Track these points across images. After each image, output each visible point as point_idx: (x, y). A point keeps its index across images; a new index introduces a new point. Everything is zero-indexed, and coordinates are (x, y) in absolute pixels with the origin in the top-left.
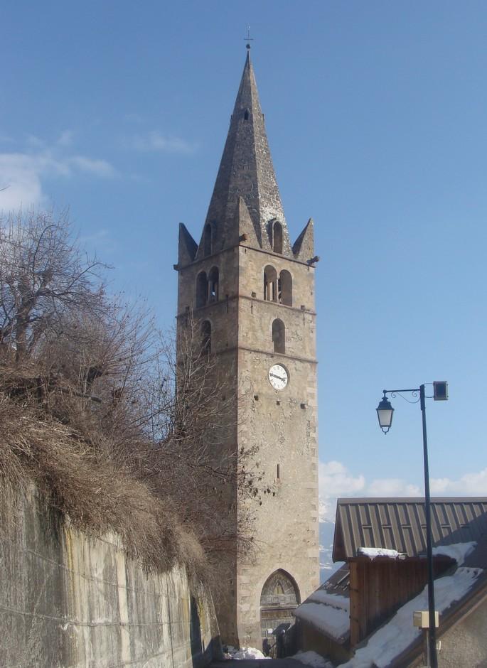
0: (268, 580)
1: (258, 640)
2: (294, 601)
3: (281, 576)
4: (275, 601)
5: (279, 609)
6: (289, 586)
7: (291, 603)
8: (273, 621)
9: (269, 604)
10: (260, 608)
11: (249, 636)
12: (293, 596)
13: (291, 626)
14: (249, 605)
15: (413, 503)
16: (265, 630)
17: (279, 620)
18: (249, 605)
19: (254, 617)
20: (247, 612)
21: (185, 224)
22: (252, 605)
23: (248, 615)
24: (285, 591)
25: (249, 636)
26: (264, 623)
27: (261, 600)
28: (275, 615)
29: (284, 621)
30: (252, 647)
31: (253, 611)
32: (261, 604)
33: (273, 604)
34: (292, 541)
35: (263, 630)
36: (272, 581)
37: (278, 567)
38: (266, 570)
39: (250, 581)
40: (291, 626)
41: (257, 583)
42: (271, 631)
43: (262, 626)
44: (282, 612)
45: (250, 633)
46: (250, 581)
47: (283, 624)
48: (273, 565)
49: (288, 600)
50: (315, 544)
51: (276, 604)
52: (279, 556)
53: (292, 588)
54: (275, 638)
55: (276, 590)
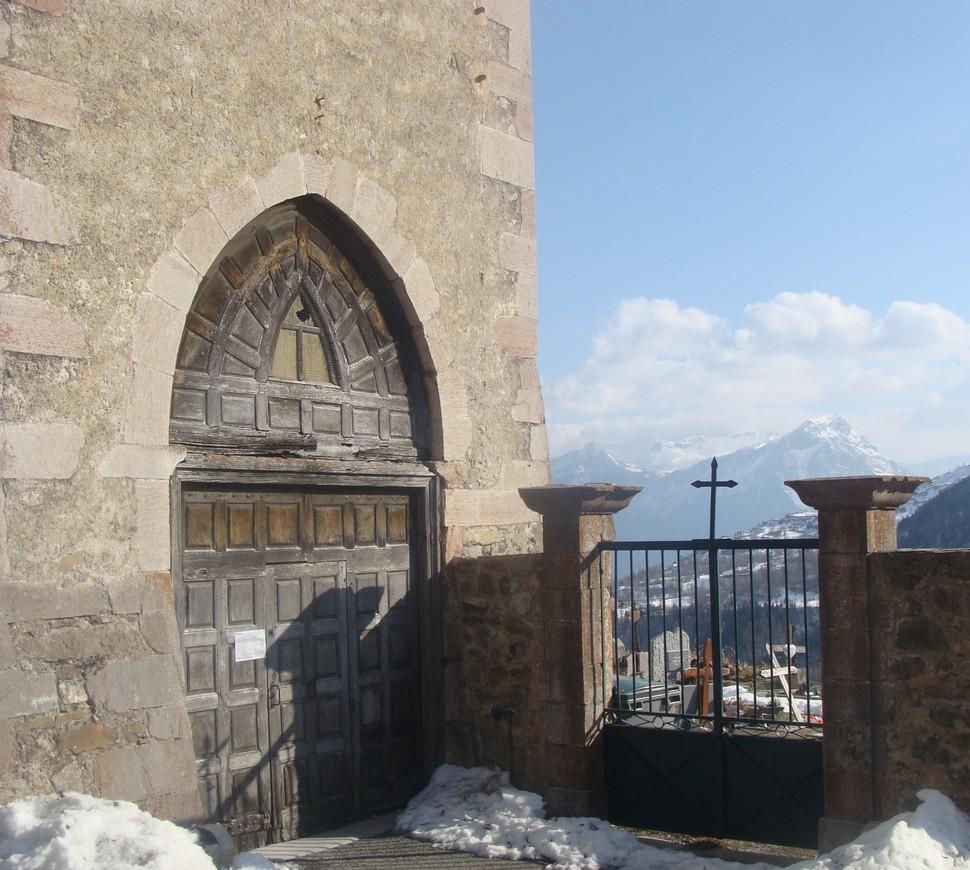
0: (232, 264)
1: (159, 726)
2: (398, 439)
3: (324, 259)
4: (282, 426)
5: (313, 487)
6: (372, 339)
7: (384, 455)
8: (267, 572)
9: (239, 446)
10: (170, 461)
11: (76, 696)
12: (394, 404)
13: (384, 609)
14: (71, 432)
15: (373, 588)
16: (211, 636)
17: (307, 569)
18: (71, 432)
19: (124, 530)
20: (58, 492)
21: (339, 201)
22: (100, 433)
23: (64, 517)
24: (348, 369)
25: (76, 696)
26: (201, 587)
27: (177, 408)
28: (281, 533)
29: (338, 571)
30: (101, 788)
31: (109, 485)
32: (180, 438)
33: (269, 448)
34: (389, 38)
35: (195, 637)
36: (257, 277)
37: (295, 178)
38: (217, 181)
39: (88, 232)
40: (384, 609)
41: (147, 257)
42: (251, 645)
43: (186, 605)
44: (327, 507)
45: (97, 662)
46: (88, 232)
47: (334, 592)
48: (269, 159)
49: (365, 433)
50: (513, 105)
51: (283, 448)
52: (304, 105)
53: (389, 350)
54: (286, 693)
55: (286, 343)
